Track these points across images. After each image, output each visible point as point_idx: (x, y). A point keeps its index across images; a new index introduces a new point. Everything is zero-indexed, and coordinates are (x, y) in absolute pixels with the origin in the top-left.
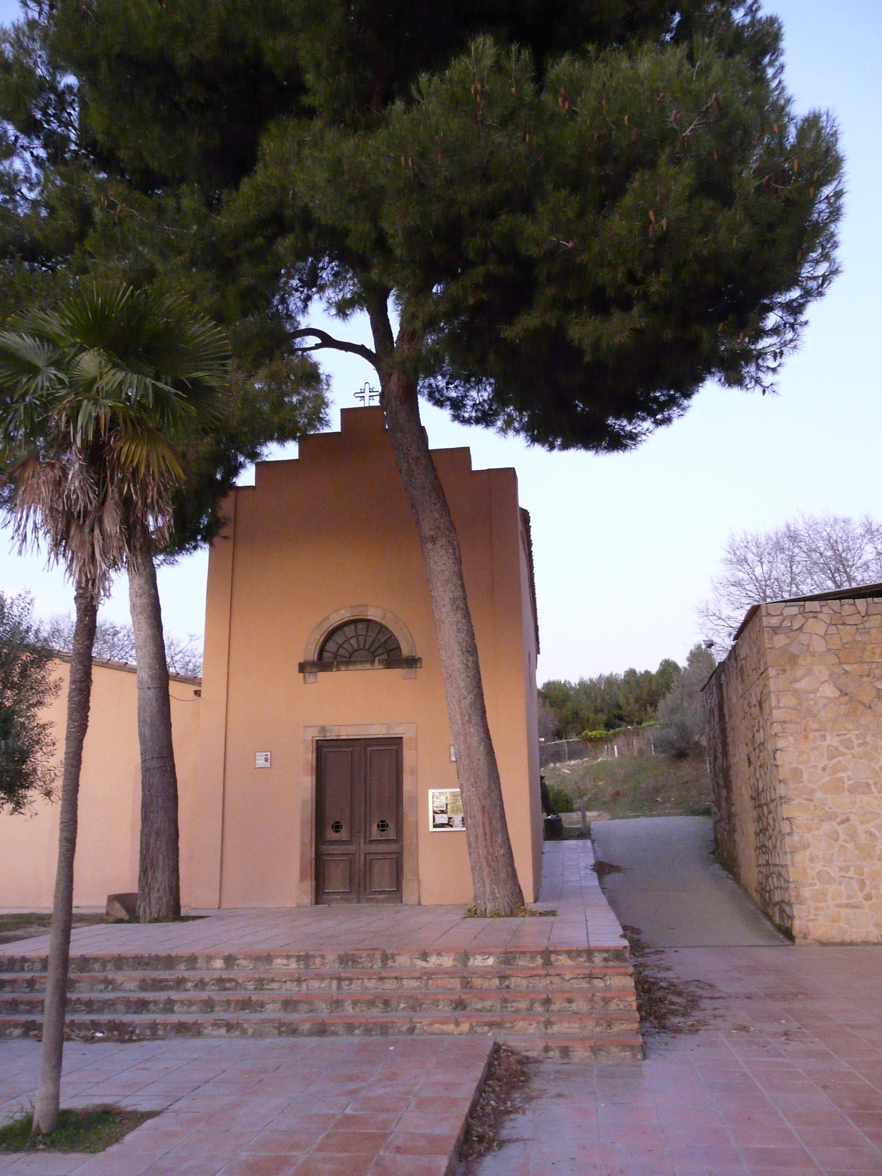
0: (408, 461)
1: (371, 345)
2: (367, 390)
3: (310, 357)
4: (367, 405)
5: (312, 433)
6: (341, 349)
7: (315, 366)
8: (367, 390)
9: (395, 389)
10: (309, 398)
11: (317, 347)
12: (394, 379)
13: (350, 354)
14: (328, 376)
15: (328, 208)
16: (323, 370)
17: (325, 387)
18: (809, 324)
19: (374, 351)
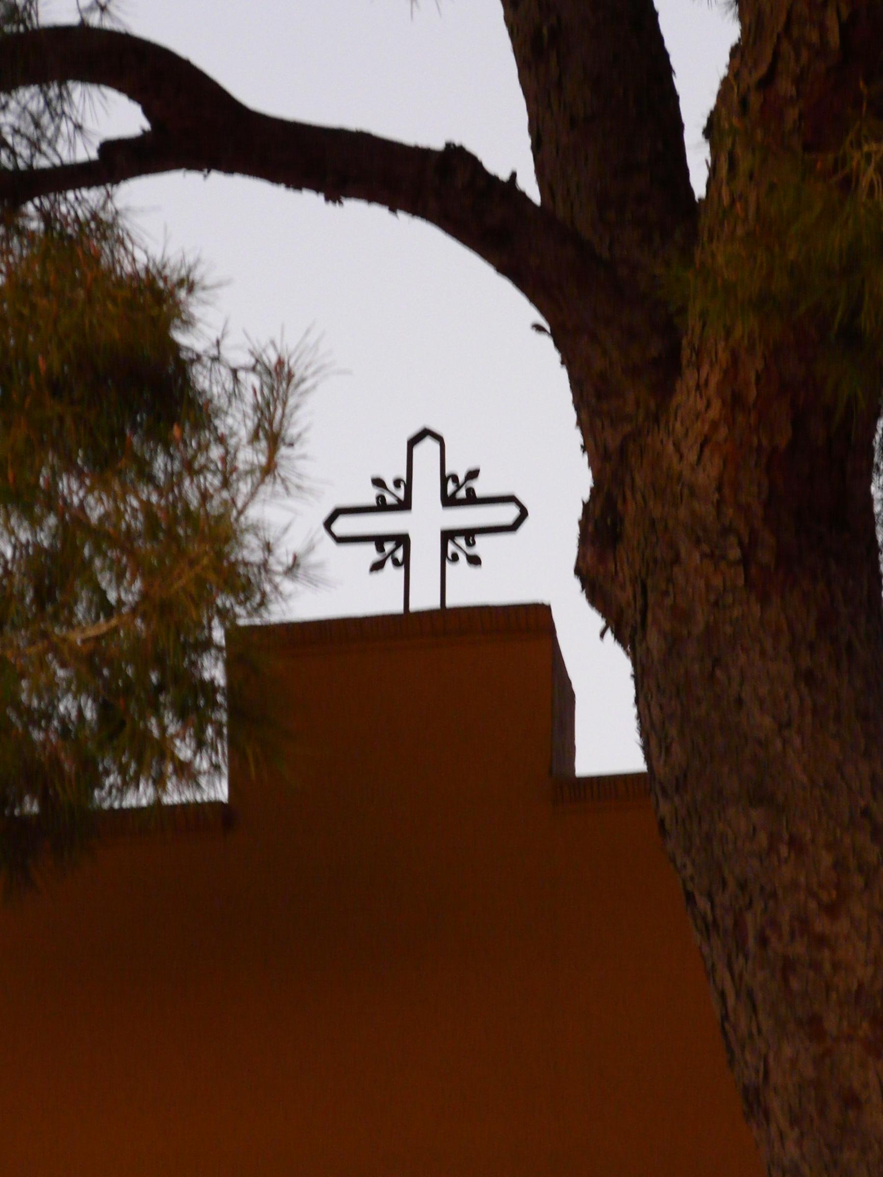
0: (814, 1026)
1: (507, 150)
2: (426, 489)
3: (104, 228)
4: (425, 599)
5: (141, 796)
6: (295, 179)
7: (157, 300)
8: (426, 489)
9: (707, 475)
10: (104, 536)
11: (120, 161)
12: (696, 399)
13: (364, 220)
14: (279, 376)
15: (850, 222)
16: (222, 331)
17: (249, 456)
18: (368, 567)
19: (530, 187)
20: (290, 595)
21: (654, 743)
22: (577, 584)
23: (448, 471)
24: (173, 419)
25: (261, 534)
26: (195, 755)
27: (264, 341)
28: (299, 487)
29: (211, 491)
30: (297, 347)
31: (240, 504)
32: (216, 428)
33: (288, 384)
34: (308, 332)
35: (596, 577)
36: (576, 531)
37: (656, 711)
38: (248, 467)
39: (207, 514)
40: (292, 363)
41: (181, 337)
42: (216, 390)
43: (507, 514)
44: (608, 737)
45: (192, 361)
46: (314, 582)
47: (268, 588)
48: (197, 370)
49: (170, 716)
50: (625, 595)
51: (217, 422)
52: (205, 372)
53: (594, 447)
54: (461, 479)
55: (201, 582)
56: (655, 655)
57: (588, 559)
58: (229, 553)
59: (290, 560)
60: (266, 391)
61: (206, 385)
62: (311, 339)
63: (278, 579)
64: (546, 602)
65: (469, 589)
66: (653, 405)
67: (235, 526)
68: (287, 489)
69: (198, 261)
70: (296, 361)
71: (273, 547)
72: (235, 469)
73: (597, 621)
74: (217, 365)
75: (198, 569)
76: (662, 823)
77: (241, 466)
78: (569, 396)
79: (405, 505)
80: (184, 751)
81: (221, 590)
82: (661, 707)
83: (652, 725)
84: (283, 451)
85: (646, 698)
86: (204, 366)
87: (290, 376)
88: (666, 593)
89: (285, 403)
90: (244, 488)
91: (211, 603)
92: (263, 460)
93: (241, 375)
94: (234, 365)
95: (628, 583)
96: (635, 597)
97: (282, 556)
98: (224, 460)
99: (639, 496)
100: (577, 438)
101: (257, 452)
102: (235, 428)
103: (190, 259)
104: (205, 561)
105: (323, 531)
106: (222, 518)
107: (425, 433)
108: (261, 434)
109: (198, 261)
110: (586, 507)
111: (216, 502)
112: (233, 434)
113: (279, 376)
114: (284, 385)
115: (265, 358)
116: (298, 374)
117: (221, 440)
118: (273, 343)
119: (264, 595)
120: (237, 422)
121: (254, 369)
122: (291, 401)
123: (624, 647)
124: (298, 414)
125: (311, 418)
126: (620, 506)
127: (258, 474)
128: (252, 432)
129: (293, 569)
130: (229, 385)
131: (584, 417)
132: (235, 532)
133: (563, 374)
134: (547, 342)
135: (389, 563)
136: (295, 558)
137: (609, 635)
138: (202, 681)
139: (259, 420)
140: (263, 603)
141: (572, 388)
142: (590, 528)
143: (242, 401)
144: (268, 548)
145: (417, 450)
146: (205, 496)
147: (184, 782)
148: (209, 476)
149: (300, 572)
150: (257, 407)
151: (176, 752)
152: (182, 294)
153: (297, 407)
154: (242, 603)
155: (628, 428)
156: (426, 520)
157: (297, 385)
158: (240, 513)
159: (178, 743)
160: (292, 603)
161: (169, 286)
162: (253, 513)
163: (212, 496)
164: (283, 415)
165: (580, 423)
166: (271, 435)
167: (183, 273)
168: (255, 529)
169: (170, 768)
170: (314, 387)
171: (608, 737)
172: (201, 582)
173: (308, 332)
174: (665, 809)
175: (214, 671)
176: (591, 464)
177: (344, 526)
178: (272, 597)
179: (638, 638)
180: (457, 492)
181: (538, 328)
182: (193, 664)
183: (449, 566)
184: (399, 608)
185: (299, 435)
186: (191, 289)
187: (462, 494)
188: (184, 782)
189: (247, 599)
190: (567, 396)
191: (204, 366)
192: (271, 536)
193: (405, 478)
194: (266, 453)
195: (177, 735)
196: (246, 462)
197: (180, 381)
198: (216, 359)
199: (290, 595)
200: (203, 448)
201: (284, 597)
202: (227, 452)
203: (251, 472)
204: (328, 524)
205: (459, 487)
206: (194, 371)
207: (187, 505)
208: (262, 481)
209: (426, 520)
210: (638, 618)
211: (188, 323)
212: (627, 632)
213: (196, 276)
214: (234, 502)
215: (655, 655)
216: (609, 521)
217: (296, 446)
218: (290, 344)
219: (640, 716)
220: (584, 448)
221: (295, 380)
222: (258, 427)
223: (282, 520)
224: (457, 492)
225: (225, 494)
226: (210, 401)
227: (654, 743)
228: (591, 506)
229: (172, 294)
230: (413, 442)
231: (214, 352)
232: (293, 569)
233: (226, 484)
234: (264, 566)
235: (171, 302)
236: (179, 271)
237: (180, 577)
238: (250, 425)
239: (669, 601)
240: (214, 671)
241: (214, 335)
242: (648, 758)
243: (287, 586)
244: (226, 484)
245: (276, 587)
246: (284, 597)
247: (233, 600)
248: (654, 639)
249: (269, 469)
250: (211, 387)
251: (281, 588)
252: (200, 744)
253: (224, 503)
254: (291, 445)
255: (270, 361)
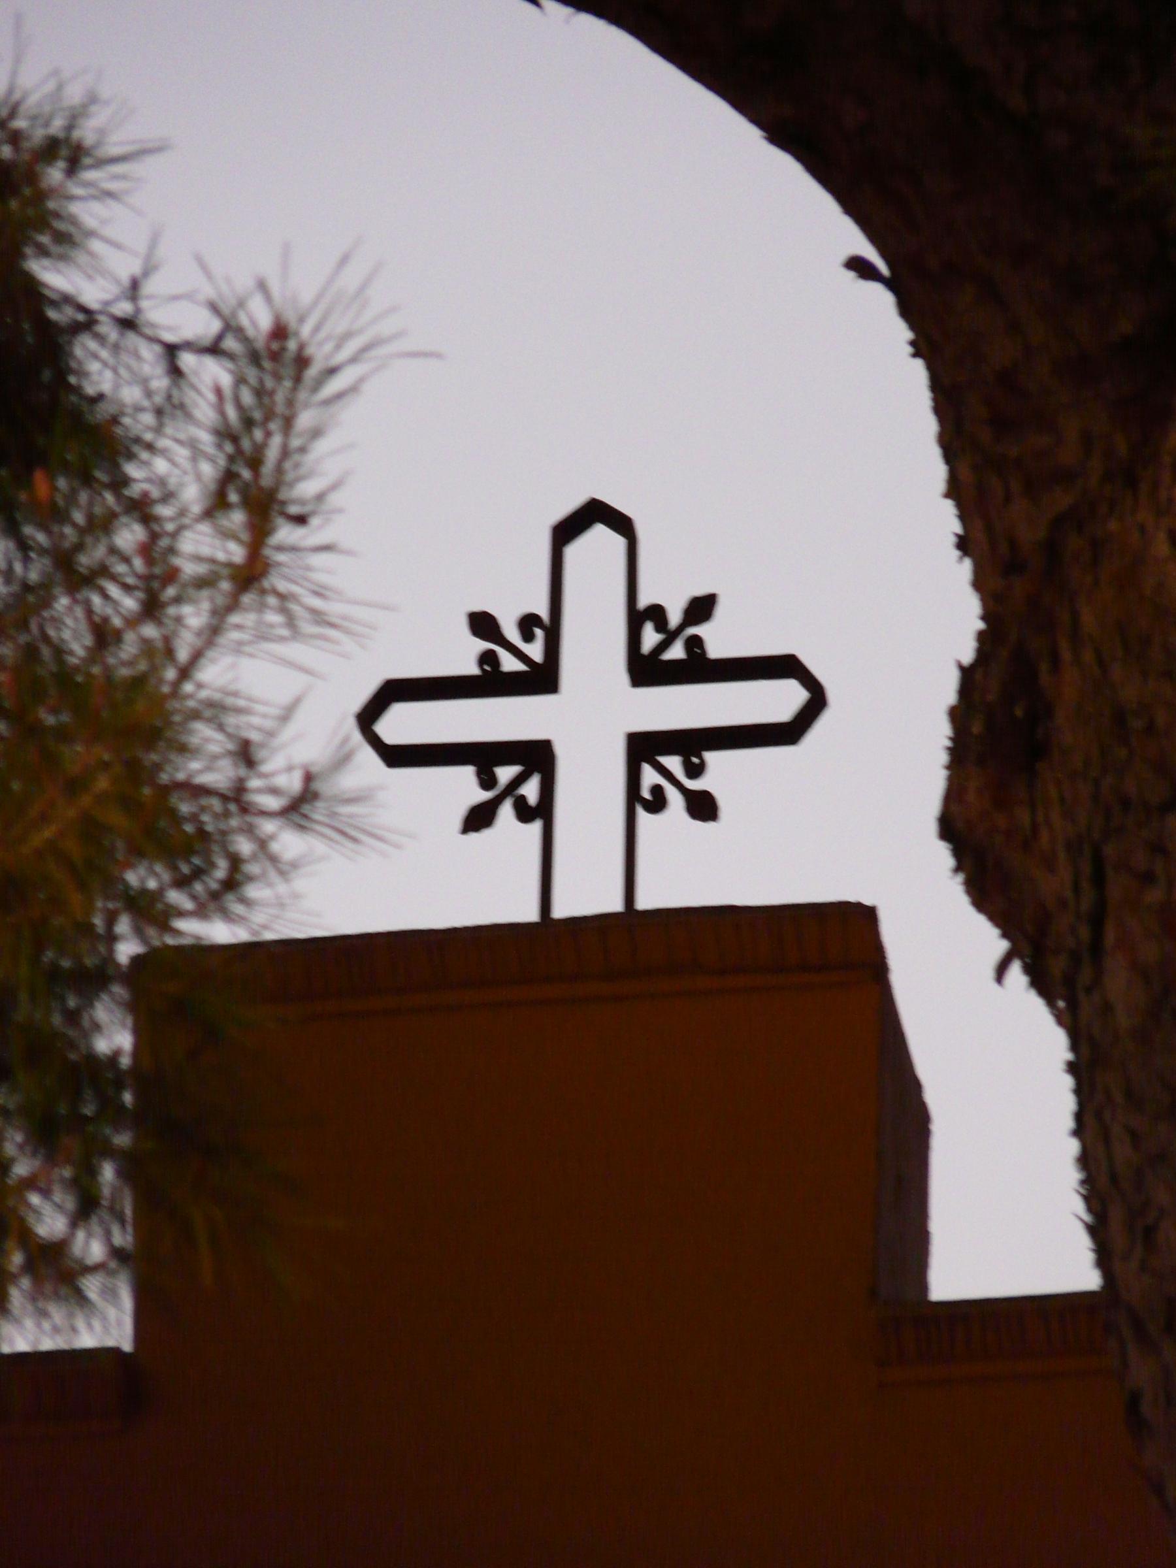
2: (594, 643)
4: (589, 891)
8: (594, 643)
17: (203, 545)
20: (295, 865)
21: (1117, 1215)
22: (942, 855)
23: (643, 602)
24: (30, 460)
25: (231, 720)
26: (74, 1224)
27: (244, 281)
28: (318, 617)
29: (117, 622)
30: (316, 303)
31: (183, 655)
32: (126, 481)
33: (298, 379)
34: (344, 260)
35: (985, 839)
36: (941, 732)
37: (1123, 1151)
38: (201, 569)
39: (108, 671)
40: (306, 331)
41: (54, 277)
42: (131, 394)
43: (778, 700)
44: (1007, 1210)
45: (77, 328)
46: (346, 834)
47: (244, 847)
48: (85, 348)
49: (19, 1138)
50: (1054, 883)
51: (132, 470)
52: (104, 354)
53: (985, 542)
54: (674, 618)
55: (91, 830)
56: (1123, 1020)
57: (971, 797)
58: (158, 767)
59: (293, 783)
60: (247, 398)
61: (106, 387)
62: (351, 278)
63: (268, 827)
64: (867, 902)
65: (686, 870)
66: (1122, 447)
67: (173, 704)
68: (291, 622)
69: (92, 99)
70: (317, 329)
71: (259, 754)
72: (172, 575)
73: (988, 941)
74: (131, 338)
75: (86, 800)
76: (1134, 1400)
77: (189, 569)
78: (930, 426)
79: (542, 679)
80: (50, 1220)
81: (137, 853)
82: (1135, 1137)
83: (1114, 1178)
84: (285, 533)
85: (1099, 1115)
86: (101, 339)
87: (302, 362)
88: (1148, 878)
89: (288, 423)
90: (194, 616)
91: (111, 884)
92: (236, 553)
93: (187, 360)
94: (170, 338)
95: (1062, 855)
96: (1076, 888)
97: (280, 772)
98: (146, 550)
99: (1088, 656)
100: (946, 520)
101: (227, 535)
102: (172, 482)
103: (74, 94)
104: (102, 783)
105: (357, 737)
106: (138, 682)
107: (594, 513)
108: (233, 497)
109: (92, 99)
110: (967, 674)
111: (129, 647)
112: (168, 496)
113: (277, 364)
114: (288, 384)
115: (244, 321)
116: (320, 354)
117: (141, 509)
118: (262, 286)
119: (236, 861)
120: (178, 466)
121: (214, 349)
122: (305, 419)
123: (1050, 1002)
124: (321, 447)
125: (348, 457)
126: (1045, 676)
127: (225, 585)
128: (213, 487)
129: (299, 807)
130: (161, 382)
131: (965, 473)
132: (166, 717)
133: (915, 377)
134: (879, 300)
135: (506, 811)
136: (309, 778)
137: (1016, 974)
138: (92, 1059)
139: (231, 459)
140: (232, 884)
141: (939, 410)
142: (976, 728)
143: (188, 416)
144: (246, 754)
145: (573, 552)
146: (104, 636)
147: (48, 1287)
148: (114, 590)
149: (318, 812)
150: (225, 434)
151: (31, 1219)
152: (54, 174)
153: (316, 433)
154: (182, 883)
155: (1062, 500)
156: (592, 714)
157: (319, 383)
158: (185, 673)
159: (35, 1199)
160: (300, 883)
161: (26, 157)
162: (214, 674)
163: (118, 636)
164: (285, 453)
165: (954, 490)
166: (256, 496)
167: (57, 126)
168: (215, 711)
169: (17, 1259)
170: (353, 389)
171: (1007, 1210)
172: (91, 830)
173: (344, 260)
174: (1143, 1373)
175: (114, 1036)
176: (978, 584)
177: (404, 724)
178: (253, 868)
179: (1085, 975)
180: (666, 650)
181: (858, 266)
182: (73, 1017)
183: (643, 817)
184: (530, 913)
185: (320, 497)
186: (74, 165)
187: (677, 652)
188: (48, 1287)
189: (198, 873)
190: (925, 425)
191: (101, 339)
192: (251, 726)
193: (543, 612)
194: (245, 536)
195: (30, 1183)
196: (198, 559)
197: (47, 375)
198: (128, 324)
199: (295, 865)
200: (102, 525)
201: (284, 869)
202: (154, 537)
203: (203, 583)
204: (368, 717)
205: (670, 638)
206: (78, 351)
207: (59, 651)
208: (233, 606)
209: (592, 714)
210: (1084, 933)
211: (67, 241)
212: (1057, 966)
213: (86, 133)
214: (170, 653)
215: (1123, 1020)
216: (1019, 712)
217: (314, 521)
218: (302, 287)
219: (1084, 1160)
220: (964, 545)
221: (312, 372)
222: (229, 477)
223: (276, 691)
224: (666, 650)
225: (150, 631)
226: (115, 420)
227: (1117, 1215)
228: (978, 676)
229: (32, 178)
230: (567, 531)
231: (124, 308)
232: (299, 807)
233: (152, 608)
234: (237, 797)
235: (27, 191)
236: (47, 124)
237: (44, 818)
238: (209, 471)
239: (1154, 896)
240: (114, 1036)
241: (125, 267)
242: (1104, 1259)
243: (289, 843)
244: (152, 608)
245: (263, 844)
246: (284, 869)
247: (166, 876)
248: (1118, 981)
249: (250, 576)
250: (117, 387)
251: (275, 847)
252: (87, 1206)
253: (148, 648)
254: (301, 520)
255: (254, 323)
